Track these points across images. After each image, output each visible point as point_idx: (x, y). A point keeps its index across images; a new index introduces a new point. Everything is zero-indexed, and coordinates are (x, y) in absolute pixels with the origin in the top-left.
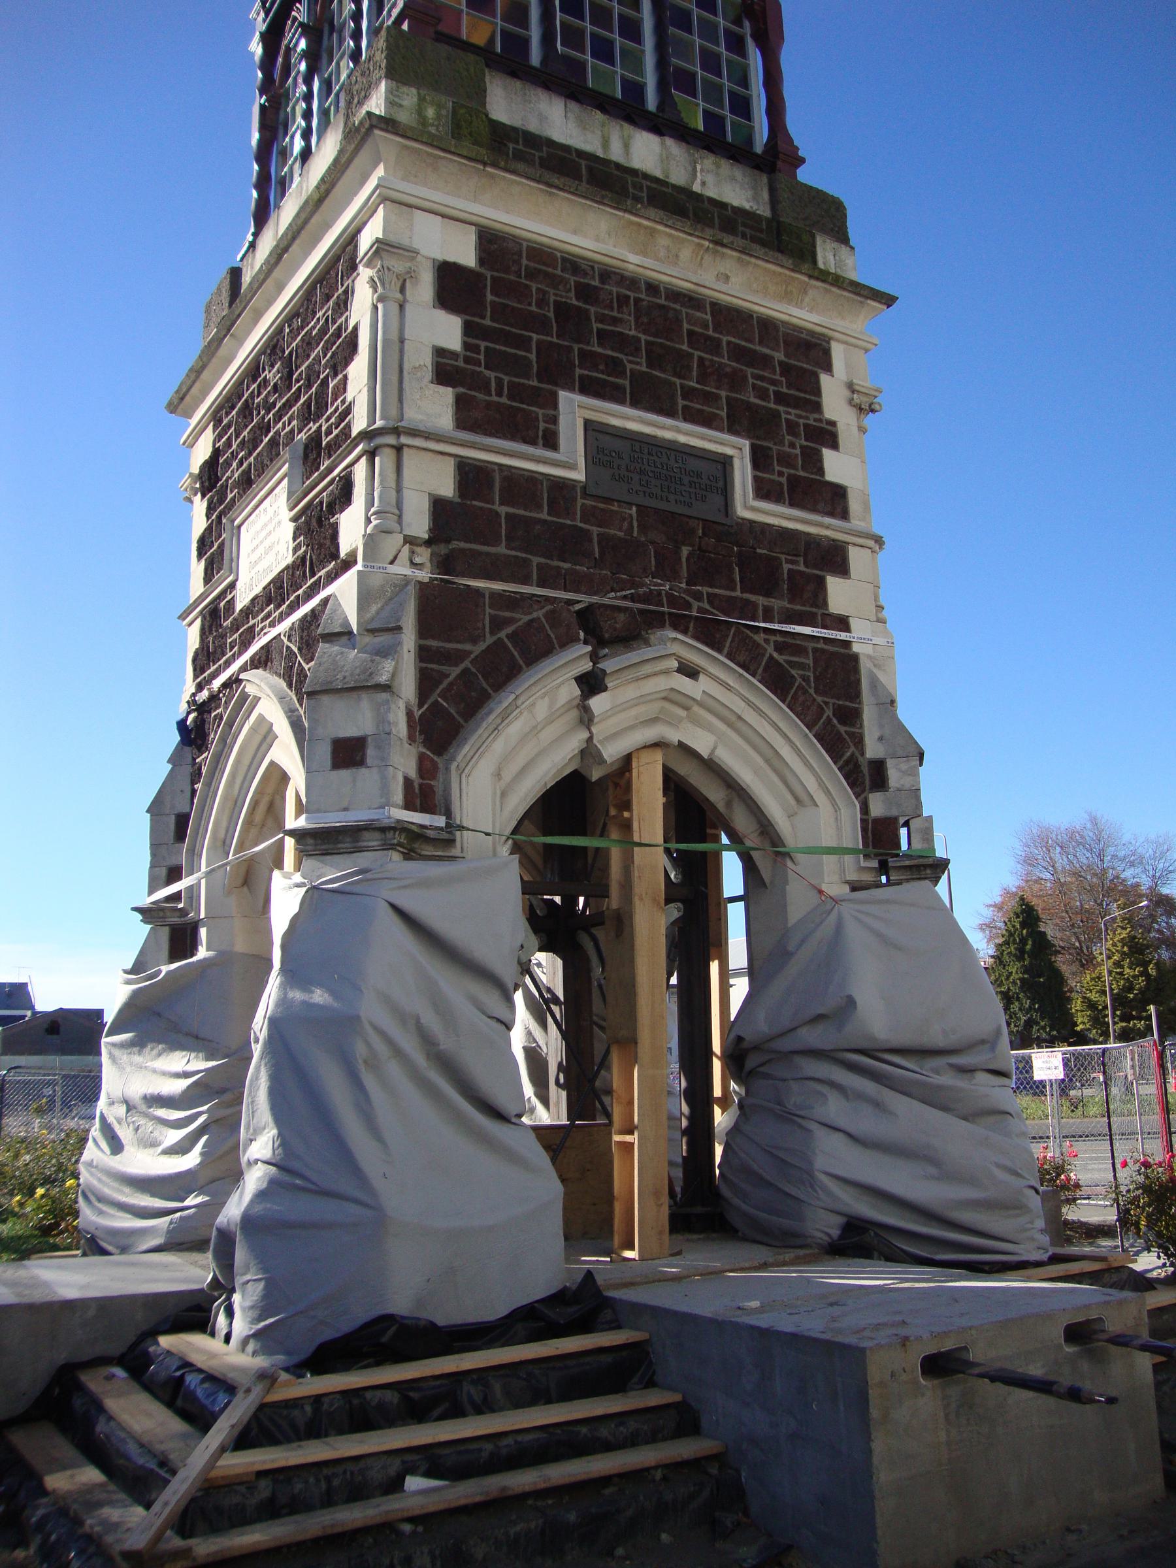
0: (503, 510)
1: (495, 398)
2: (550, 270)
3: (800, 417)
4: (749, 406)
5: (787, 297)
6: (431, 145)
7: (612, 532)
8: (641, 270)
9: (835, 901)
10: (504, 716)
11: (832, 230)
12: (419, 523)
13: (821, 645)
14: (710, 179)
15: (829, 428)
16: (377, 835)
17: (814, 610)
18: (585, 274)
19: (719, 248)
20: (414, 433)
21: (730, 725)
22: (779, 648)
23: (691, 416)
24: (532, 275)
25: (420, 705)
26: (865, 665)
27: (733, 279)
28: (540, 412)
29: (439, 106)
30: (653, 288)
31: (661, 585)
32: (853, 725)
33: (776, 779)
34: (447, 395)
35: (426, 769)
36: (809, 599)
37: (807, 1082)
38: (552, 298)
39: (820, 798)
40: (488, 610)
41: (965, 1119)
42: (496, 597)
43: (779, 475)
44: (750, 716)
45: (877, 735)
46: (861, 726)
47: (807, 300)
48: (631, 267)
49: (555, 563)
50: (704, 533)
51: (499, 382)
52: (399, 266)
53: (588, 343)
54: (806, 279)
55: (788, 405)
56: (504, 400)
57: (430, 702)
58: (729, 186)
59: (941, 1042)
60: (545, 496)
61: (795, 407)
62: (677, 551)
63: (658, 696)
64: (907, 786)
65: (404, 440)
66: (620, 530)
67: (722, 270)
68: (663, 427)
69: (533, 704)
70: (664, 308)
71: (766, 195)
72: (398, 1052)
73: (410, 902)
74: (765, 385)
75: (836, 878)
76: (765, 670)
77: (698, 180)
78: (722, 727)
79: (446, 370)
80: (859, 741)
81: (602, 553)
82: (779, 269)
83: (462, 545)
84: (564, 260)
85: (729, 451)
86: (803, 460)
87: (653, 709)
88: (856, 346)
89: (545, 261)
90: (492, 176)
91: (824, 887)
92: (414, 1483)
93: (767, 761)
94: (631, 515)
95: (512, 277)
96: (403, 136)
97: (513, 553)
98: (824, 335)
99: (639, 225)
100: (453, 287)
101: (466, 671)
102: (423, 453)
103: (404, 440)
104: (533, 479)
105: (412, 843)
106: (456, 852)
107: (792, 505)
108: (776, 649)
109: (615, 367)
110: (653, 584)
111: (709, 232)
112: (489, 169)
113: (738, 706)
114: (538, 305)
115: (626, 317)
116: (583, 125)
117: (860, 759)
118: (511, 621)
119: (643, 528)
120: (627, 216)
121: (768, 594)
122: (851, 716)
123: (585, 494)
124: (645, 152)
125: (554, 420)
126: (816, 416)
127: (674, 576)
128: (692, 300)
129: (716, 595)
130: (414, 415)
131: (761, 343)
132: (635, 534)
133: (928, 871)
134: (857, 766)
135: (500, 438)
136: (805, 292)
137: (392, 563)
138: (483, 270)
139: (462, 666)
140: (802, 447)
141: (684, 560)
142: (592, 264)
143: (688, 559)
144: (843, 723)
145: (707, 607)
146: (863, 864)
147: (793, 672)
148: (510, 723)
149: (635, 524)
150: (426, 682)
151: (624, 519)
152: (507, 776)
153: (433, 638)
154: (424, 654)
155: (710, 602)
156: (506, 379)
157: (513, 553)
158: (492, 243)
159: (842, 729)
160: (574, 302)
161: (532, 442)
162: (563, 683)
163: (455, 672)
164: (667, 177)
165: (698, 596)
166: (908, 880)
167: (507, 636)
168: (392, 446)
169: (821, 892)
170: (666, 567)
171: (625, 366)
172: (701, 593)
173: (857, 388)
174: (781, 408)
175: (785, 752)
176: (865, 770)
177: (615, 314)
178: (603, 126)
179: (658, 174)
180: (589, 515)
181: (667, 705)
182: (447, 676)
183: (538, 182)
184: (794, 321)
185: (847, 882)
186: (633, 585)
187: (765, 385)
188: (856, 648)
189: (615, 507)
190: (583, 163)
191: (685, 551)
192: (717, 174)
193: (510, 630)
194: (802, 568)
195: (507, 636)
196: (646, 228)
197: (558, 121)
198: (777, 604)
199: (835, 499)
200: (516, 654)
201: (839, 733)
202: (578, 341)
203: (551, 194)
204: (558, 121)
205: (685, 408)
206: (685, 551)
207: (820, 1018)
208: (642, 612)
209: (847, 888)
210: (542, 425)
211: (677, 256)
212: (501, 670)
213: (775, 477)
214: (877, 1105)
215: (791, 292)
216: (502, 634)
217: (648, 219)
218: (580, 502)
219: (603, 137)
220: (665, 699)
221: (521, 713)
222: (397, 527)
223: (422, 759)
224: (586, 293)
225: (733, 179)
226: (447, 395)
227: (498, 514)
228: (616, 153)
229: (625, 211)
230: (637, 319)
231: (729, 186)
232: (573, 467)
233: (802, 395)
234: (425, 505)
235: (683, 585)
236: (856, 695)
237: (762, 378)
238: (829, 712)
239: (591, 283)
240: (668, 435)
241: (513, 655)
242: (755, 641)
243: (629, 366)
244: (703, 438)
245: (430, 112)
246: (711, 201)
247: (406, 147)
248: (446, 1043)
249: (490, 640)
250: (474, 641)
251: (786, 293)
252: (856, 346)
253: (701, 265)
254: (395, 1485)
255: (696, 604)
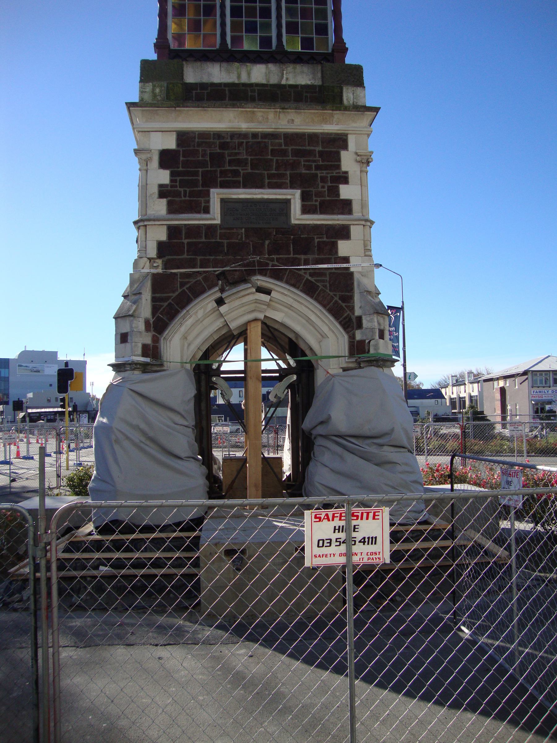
0: (186, 241)
1: (183, 198)
2: (208, 140)
3: (328, 173)
4: (301, 175)
5: (325, 121)
6: (152, 107)
7: (233, 241)
8: (249, 130)
9: (333, 376)
10: (184, 317)
11: (353, 81)
12: (152, 252)
13: (334, 271)
14: (290, 76)
15: (344, 175)
16: (129, 366)
17: (330, 256)
18: (224, 138)
19: (285, 110)
20: (149, 220)
21: (289, 309)
22: (311, 275)
23: (272, 186)
24: (199, 145)
25: (153, 318)
26: (356, 276)
27: (296, 120)
28: (202, 199)
29: (161, 87)
30: (255, 135)
31: (255, 258)
32: (348, 302)
33: (311, 328)
34: (164, 202)
35: (156, 340)
36: (329, 251)
37: (321, 447)
38: (209, 152)
39: (330, 334)
40: (179, 280)
41: (377, 465)
42: (183, 275)
43: (316, 201)
44: (296, 305)
45: (359, 306)
46: (354, 302)
47: (335, 119)
48: (244, 130)
49: (208, 257)
50: (276, 233)
51: (185, 191)
52: (144, 156)
53: (224, 167)
54: (331, 112)
55: (321, 170)
56: (187, 198)
57: (156, 316)
58: (300, 76)
59: (369, 434)
60: (204, 232)
61: (325, 170)
62: (263, 244)
63: (253, 302)
64: (369, 327)
65: (146, 223)
66: (237, 239)
67: (290, 118)
68: (256, 194)
69: (197, 312)
70: (258, 143)
71: (319, 75)
72: (128, 438)
73: (139, 388)
74: (310, 163)
75: (336, 366)
76: (304, 285)
77: (285, 78)
78: (286, 310)
79: (163, 192)
80: (352, 309)
81: (228, 250)
82: (316, 111)
83: (170, 257)
84: (214, 134)
85: (289, 197)
86: (328, 193)
87: (252, 307)
88: (362, 134)
89: (204, 137)
90: (179, 111)
91: (330, 371)
92: (101, 568)
93: (307, 321)
94: (242, 233)
95: (191, 148)
96: (141, 107)
97: (190, 257)
98: (344, 134)
99: (246, 111)
100: (166, 159)
101: (170, 304)
102: (154, 226)
103: (146, 223)
104: (199, 227)
105: (144, 368)
106: (165, 368)
107: (321, 213)
108: (310, 276)
109: (236, 173)
110: (250, 258)
111: (277, 105)
112: (177, 109)
113: (289, 301)
114: (202, 156)
115: (241, 151)
116: (228, 72)
117: (352, 316)
118: (188, 282)
119: (247, 236)
120: (240, 109)
121: (305, 253)
122: (348, 299)
123: (221, 229)
124: (259, 74)
125: (208, 202)
126: (338, 171)
127: (261, 253)
128: (273, 136)
129: (280, 258)
130: (151, 212)
131: (309, 145)
132: (244, 239)
133: (375, 362)
134: (350, 319)
135: (186, 213)
136: (333, 116)
137: (143, 269)
138: (179, 149)
139: (168, 302)
140: (329, 187)
141: (266, 246)
142: (227, 132)
143: (268, 245)
144: (344, 302)
145: (276, 263)
146: (347, 360)
147: (318, 284)
148: (186, 321)
149: (244, 236)
150: (155, 310)
151: (239, 234)
152: (190, 338)
153: (158, 293)
154: (154, 299)
155: (277, 261)
156: (188, 190)
157: (190, 257)
158: (183, 137)
159: (344, 305)
160: (219, 151)
161: (199, 212)
162: (209, 302)
163: (166, 304)
164: (269, 82)
165: (272, 260)
166: (366, 366)
167: (187, 288)
168: (143, 226)
169: (328, 372)
170: (258, 250)
171: (240, 172)
172: (274, 258)
173: (359, 154)
174: (318, 172)
175: (313, 318)
176: (354, 320)
177: (237, 151)
178: (238, 68)
179: (264, 82)
180: (222, 236)
181: (258, 305)
182: (163, 306)
183: (199, 107)
184: (326, 131)
185: (342, 368)
186: (242, 260)
187: (310, 163)
188: (352, 270)
189: (235, 231)
190: (227, 89)
191: (267, 242)
192: (295, 72)
193: (188, 286)
194: (325, 239)
195: (187, 288)
196: (250, 111)
197: (217, 74)
198: (310, 257)
199: (346, 206)
200: (190, 294)
201: (341, 306)
202: (219, 167)
203: (205, 110)
204: (217, 74)
205: (269, 183)
206: (267, 242)
207: (322, 423)
208: (245, 270)
209: (341, 370)
210: (203, 204)
211: (268, 118)
212: (184, 301)
213: (314, 203)
214: (341, 457)
215: (326, 118)
216: (185, 288)
217: (249, 108)
218: (219, 231)
219: (238, 73)
220: (255, 302)
221: (191, 316)
222: (144, 255)
223: (154, 336)
224: (224, 146)
225: (302, 72)
226: (164, 202)
227: (183, 243)
228: (244, 79)
229: (238, 108)
230: (247, 150)
231: (300, 76)
232: (214, 219)
233: (330, 163)
234: (155, 245)
235: (267, 256)
236: (352, 290)
237: (309, 161)
238: (337, 299)
239: (224, 141)
240: (259, 196)
241: (189, 295)
242: (299, 274)
243: (242, 172)
244: (276, 194)
245: (157, 90)
246: (291, 86)
247: (144, 110)
248: (151, 434)
249: (180, 291)
250: (174, 292)
251: (323, 119)
252: (362, 134)
253: (279, 118)
254: (96, 568)
255: (271, 263)
